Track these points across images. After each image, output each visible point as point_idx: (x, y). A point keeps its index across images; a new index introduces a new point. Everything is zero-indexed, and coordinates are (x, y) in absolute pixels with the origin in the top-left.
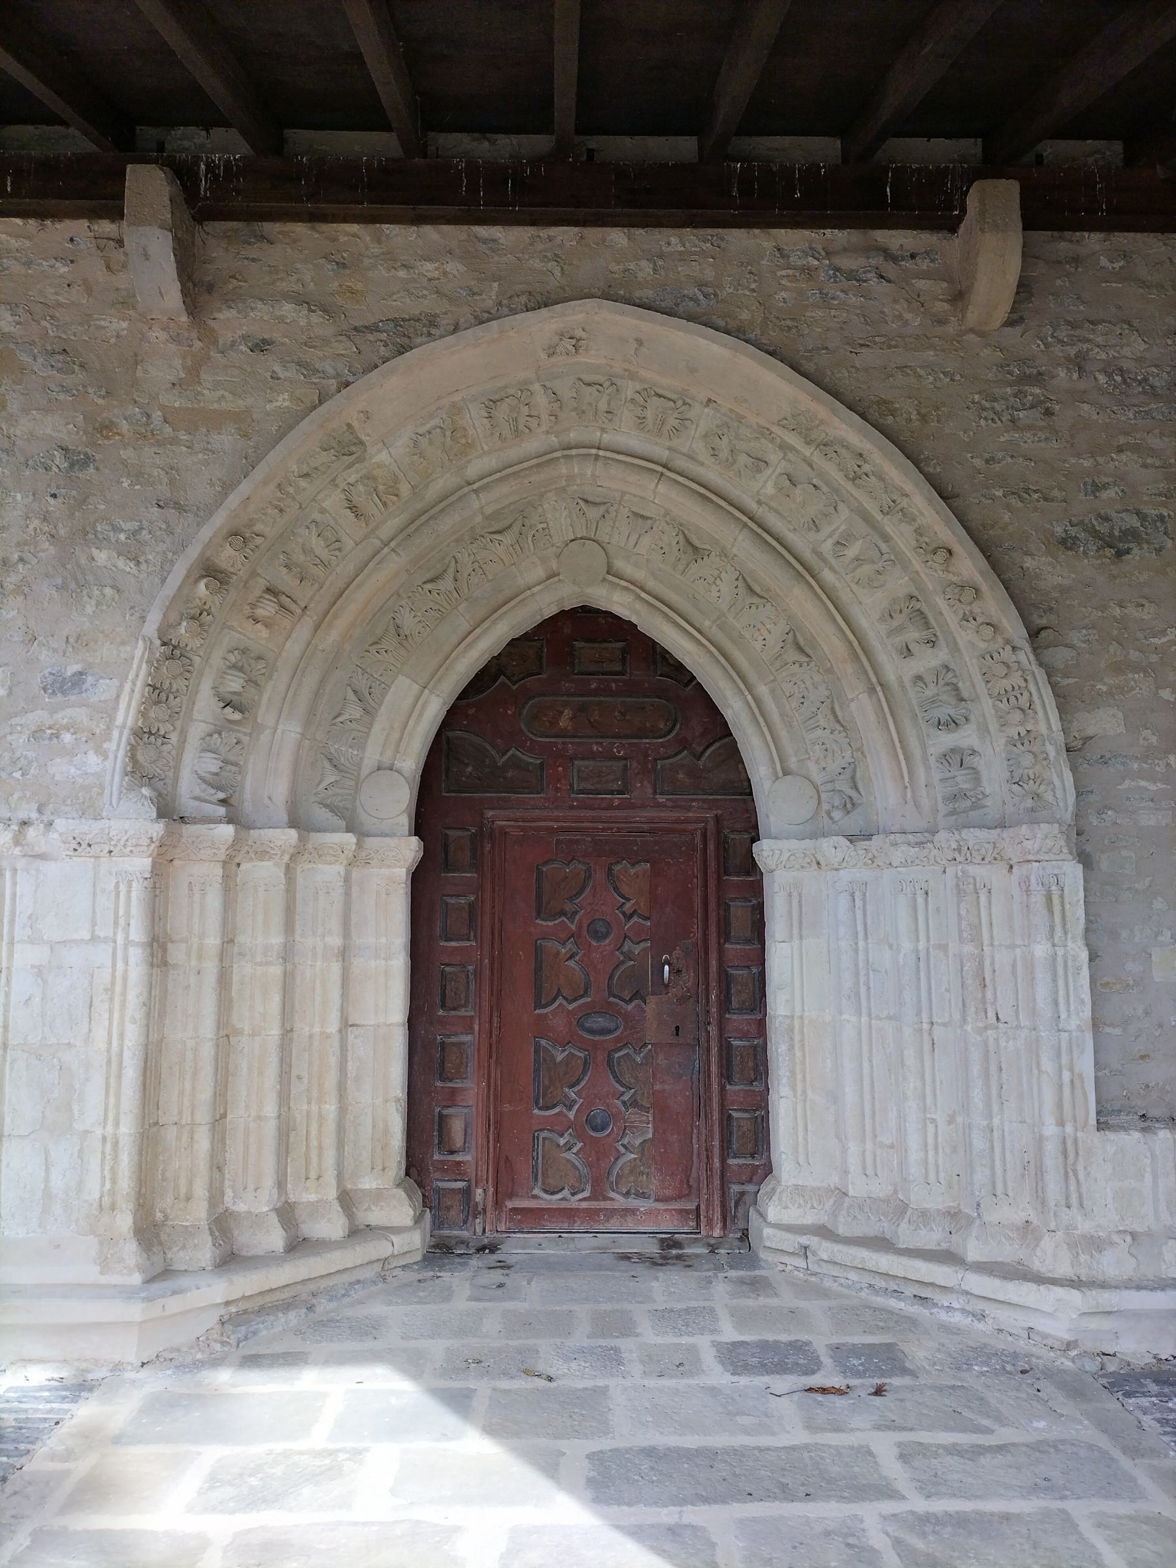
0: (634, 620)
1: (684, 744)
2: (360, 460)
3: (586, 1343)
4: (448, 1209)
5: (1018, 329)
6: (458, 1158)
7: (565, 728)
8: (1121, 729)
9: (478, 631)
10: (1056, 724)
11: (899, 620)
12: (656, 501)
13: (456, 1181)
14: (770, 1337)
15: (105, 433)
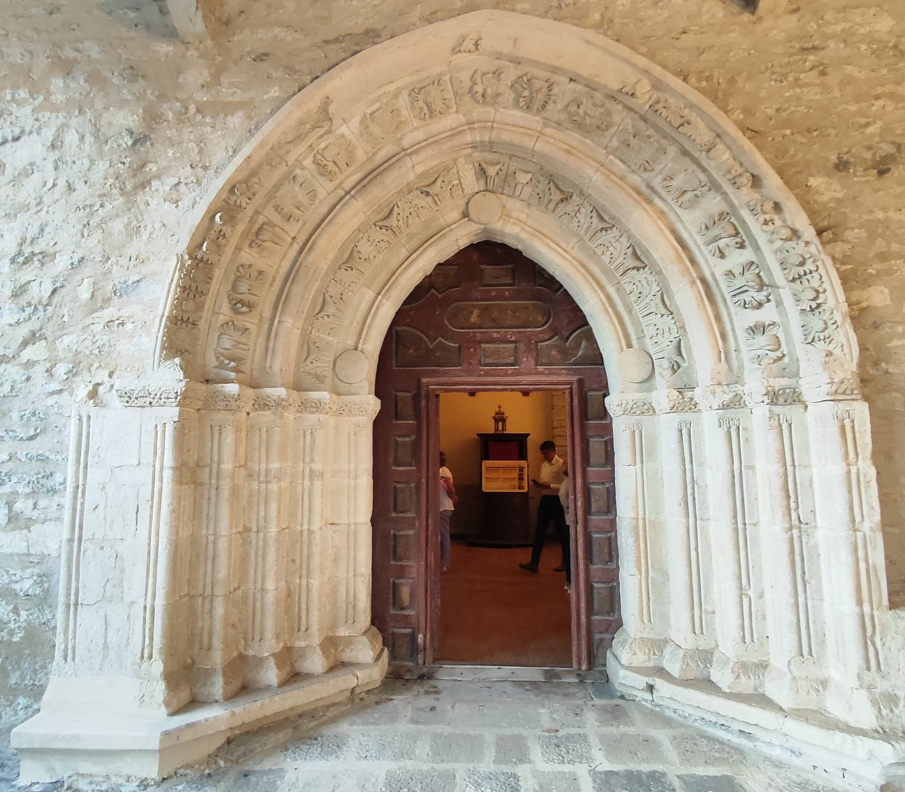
0: (520, 247)
1: (555, 332)
2: (329, 132)
3: (492, 768)
4: (400, 647)
5: (795, 16)
6: (406, 613)
7: (475, 323)
8: (889, 302)
9: (414, 255)
10: (841, 297)
11: (715, 232)
12: (534, 160)
13: (405, 628)
14: (633, 766)
15: (157, 120)
